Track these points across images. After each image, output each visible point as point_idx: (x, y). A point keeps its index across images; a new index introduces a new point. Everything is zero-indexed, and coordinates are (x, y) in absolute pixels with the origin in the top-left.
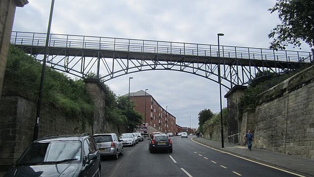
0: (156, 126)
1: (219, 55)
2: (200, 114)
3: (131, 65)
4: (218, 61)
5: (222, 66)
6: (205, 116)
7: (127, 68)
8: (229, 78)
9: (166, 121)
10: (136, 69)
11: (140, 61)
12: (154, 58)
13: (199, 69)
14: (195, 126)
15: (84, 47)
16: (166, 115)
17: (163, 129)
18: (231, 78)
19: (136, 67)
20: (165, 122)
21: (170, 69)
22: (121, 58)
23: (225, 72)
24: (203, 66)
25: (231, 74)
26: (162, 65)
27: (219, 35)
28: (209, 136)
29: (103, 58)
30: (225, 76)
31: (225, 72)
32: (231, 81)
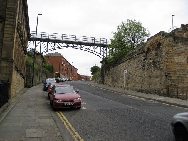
0: (65, 74)
1: (36, 36)
2: (92, 68)
3: (56, 46)
4: (92, 45)
5: (99, 47)
6: (94, 69)
7: (55, 48)
8: (102, 54)
9: (71, 72)
10: (59, 48)
11: (60, 44)
12: (54, 41)
13: (88, 49)
14: (89, 74)
15: (35, 37)
16: (71, 68)
17: (69, 76)
18: (104, 53)
19: (65, 46)
20: (66, 73)
21: (75, 48)
22: (51, 42)
23: (100, 51)
24: (91, 48)
25: (104, 52)
26: (71, 46)
27: (39, 14)
28: (94, 81)
29: (42, 42)
30: (100, 53)
31: (100, 51)
32: (103, 56)
